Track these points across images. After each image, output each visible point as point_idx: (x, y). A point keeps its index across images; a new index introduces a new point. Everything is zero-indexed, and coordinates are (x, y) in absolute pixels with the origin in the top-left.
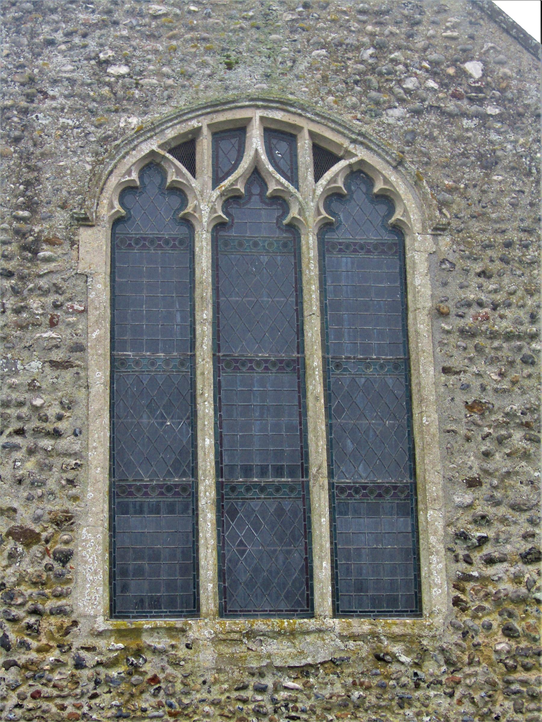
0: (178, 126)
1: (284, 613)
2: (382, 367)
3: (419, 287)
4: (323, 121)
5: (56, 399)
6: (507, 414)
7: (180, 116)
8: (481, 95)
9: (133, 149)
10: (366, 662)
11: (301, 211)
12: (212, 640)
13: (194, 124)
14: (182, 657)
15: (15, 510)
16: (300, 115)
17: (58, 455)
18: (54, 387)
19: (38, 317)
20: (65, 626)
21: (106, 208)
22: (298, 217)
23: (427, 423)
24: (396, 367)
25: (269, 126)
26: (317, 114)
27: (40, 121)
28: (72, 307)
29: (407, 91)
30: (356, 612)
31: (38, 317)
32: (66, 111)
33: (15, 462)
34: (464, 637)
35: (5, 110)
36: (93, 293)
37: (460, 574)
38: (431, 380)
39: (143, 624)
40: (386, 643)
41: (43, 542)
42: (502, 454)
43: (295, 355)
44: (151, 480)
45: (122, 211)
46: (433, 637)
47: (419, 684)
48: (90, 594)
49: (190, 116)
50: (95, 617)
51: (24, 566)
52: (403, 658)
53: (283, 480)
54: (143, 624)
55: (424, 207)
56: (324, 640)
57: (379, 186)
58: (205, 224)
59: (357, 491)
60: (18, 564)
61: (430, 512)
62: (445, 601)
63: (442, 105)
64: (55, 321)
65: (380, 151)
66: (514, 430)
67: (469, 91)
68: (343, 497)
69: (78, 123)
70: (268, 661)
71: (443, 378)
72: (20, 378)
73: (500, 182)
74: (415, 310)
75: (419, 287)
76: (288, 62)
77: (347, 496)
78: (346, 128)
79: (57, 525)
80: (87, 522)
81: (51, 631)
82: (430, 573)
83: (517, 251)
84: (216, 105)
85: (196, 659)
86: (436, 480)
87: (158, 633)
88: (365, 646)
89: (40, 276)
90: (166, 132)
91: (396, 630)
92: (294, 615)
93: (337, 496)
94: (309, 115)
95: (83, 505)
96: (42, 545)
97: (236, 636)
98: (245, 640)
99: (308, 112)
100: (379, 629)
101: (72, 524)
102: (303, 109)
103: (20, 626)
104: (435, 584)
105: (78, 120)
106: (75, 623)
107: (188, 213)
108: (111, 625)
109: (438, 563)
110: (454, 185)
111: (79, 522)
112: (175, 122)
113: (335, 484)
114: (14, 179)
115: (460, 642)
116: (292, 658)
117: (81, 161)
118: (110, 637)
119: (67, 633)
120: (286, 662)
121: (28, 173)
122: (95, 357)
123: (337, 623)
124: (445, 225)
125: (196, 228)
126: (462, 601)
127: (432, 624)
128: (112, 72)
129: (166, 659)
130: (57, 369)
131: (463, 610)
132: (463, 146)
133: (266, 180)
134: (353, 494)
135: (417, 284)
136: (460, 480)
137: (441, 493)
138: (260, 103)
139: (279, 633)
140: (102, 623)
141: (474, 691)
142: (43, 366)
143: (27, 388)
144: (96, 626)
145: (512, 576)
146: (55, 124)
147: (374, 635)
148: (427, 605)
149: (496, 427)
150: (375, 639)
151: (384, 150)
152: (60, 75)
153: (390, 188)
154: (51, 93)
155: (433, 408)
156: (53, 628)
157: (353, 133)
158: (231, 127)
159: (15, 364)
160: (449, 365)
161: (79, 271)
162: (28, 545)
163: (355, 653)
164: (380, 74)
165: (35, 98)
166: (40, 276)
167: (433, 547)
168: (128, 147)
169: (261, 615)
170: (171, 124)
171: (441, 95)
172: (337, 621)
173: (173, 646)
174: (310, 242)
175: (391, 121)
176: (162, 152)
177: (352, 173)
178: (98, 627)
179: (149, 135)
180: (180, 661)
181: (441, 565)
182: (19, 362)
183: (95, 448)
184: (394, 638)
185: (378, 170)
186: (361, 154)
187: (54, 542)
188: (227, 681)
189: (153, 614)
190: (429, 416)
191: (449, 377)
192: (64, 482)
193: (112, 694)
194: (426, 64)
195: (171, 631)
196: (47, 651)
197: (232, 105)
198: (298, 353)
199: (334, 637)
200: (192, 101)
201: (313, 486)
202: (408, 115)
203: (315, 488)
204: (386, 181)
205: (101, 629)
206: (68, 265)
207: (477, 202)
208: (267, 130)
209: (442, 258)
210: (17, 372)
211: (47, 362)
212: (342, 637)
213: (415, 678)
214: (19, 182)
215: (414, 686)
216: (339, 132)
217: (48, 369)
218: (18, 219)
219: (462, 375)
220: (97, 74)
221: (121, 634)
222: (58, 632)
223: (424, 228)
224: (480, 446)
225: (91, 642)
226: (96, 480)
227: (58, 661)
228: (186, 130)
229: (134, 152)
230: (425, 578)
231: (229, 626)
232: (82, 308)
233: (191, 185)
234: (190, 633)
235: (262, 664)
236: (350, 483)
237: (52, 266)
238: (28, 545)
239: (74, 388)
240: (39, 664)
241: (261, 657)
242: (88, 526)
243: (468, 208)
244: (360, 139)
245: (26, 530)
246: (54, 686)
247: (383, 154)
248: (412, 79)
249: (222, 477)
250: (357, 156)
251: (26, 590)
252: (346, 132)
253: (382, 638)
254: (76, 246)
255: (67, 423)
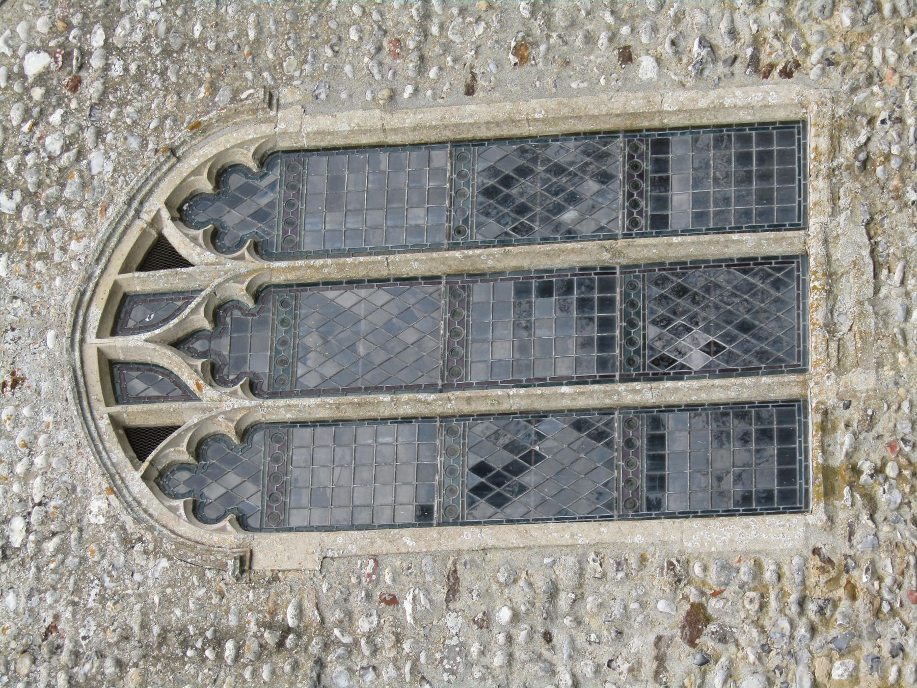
0: (107, 445)
1: (801, 292)
2: (460, 175)
3: (352, 125)
4: (107, 254)
5: (502, 593)
6: (533, 14)
7: (94, 439)
8: (76, 53)
9: (139, 504)
10: (867, 184)
11: (237, 278)
12: (839, 374)
13: (104, 424)
14: (861, 413)
15: (659, 638)
16: (97, 284)
17: (581, 585)
18: (485, 594)
19: (382, 621)
20: (819, 564)
21: (226, 537)
22: (246, 283)
23: (543, 112)
24: (460, 158)
25: (110, 328)
26: (98, 260)
27: (91, 634)
28: (369, 575)
29: (66, 148)
30: (800, 202)
31: (382, 621)
32: (76, 599)
33: (590, 643)
34: (833, 64)
35: (73, 682)
36: (350, 547)
37: (749, 70)
38: (483, 109)
39: (817, 463)
40: (842, 160)
41: (704, 599)
42: (587, 23)
43: (443, 287)
44: (617, 467)
45: (229, 517)
46: (833, 102)
47: (897, 118)
48: (779, 537)
49: (93, 428)
50: (807, 525)
51: (737, 621)
52: (862, 139)
53: (618, 298)
54: (817, 463)
55: (237, 120)
56: (838, 236)
57: (205, 185)
58: (254, 403)
59: (635, 205)
60: (734, 630)
61: (666, 107)
62: (786, 87)
63: (88, 103)
64: (388, 598)
65: (154, 179)
66: (554, 7)
67: (69, 69)
68: (643, 222)
69: (97, 582)
70: (866, 303)
71: (479, 94)
72: (470, 640)
73: (204, 27)
74: (384, 130)
75: (352, 125)
76: (15, 306)
77: (642, 216)
78: (118, 223)
79: (679, 581)
80: (675, 542)
81: (826, 582)
82: (748, 107)
83: (303, 5)
84: (79, 393)
85: (864, 395)
86: (622, 100)
87: (829, 446)
88: (846, 185)
89: (323, 621)
90: (115, 461)
91: (824, 143)
92: (804, 280)
93: (641, 229)
94: (98, 272)
95: (652, 549)
96: (707, 601)
97: (833, 345)
98: (839, 335)
99: (93, 273)
100: (824, 168)
101: (678, 561)
102: (89, 278)
103: (820, 623)
104: (763, 99)
105: (92, 582)
106: (816, 551)
107: (236, 428)
108: (818, 504)
109: (735, 96)
110: (206, 85)
111: (676, 552)
112: (101, 447)
113: (625, 232)
114: (177, 664)
115: (840, 68)
116: (863, 274)
117: (153, 574)
118: (834, 507)
119: (830, 561)
120: (868, 282)
121: (168, 646)
122: (442, 540)
123: (814, 222)
124: (265, 92)
125: (257, 419)
126: (785, 67)
127: (816, 103)
128: (20, 540)
129: (864, 434)
130: (458, 591)
131: (797, 65)
132: (149, 75)
133: (190, 330)
134: (638, 209)
135: (349, 129)
136: (622, 71)
137: (640, 94)
138: (78, 336)
139: (829, 292)
140: (817, 515)
141: (905, 52)
142: (455, 611)
143: (484, 630)
144: (819, 524)
145: (752, 8)
146: (96, 613)
147: (832, 172)
148: (791, 111)
149: (549, 28)
150: (836, 173)
151: (153, 174)
152: (21, 610)
153: (208, 167)
154: (49, 620)
155: (523, 106)
156: (823, 579)
157: (126, 213)
158: (109, 378)
159: (451, 648)
160: (463, 88)
161: (318, 568)
162: (708, 620)
163: (856, 197)
164: (40, 184)
165: (56, 643)
166: (323, 621)
167: (713, 102)
168: (136, 509)
169: (804, 320)
170: (104, 453)
171: (73, 105)
172: (811, 222)
173: (847, 426)
174: (281, 271)
175: (109, 167)
176: (146, 464)
177: (181, 219)
178: (821, 521)
179: (120, 482)
180: (868, 415)
181: (738, 92)
182: (447, 642)
183: (572, 535)
184: (835, 148)
185: (181, 183)
186: (156, 203)
187: (704, 585)
188: (894, 354)
189: (803, 458)
190: (534, 109)
191: (480, 86)
192: (621, 575)
193: (912, 500)
194: (26, 128)
195: (826, 428)
196: (854, 587)
197: (79, 373)
198: (440, 283)
199: (834, 223)
200: (70, 429)
201: (628, 257)
202: (101, 147)
203: (631, 255)
204: (196, 172)
205: (825, 518)
206: (308, 584)
207: (231, 56)
208: (114, 333)
209: (311, 98)
210: (462, 645)
211: (447, 606)
212: (834, 214)
213: (889, 122)
214: (183, 657)
215: (899, 125)
216: (124, 233)
217: (458, 605)
218: (237, 657)
219: (476, 71)
220: (23, 560)
221: (829, 492)
222: (828, 572)
223: (268, 120)
224: (576, 48)
225: (841, 530)
226: (618, 532)
227: (867, 570)
228: (113, 434)
229: (144, 502)
230: (754, 115)
231: (820, 354)
232: (371, 562)
233: (195, 425)
234: (830, 403)
235: (871, 311)
236: (623, 213)
237: (308, 605)
238: (708, 620)
239: (486, 567)
240: (872, 595)
241: (861, 313)
242: (682, 540)
243: (240, 68)
244: (135, 204)
245: (687, 620)
246: (902, 574)
247: (159, 174)
248: (47, 143)
249: (614, 376)
250: (159, 211)
251: (771, 618)
252: (124, 223)
253: (835, 164)
254: (280, 575)
255: (536, 576)
